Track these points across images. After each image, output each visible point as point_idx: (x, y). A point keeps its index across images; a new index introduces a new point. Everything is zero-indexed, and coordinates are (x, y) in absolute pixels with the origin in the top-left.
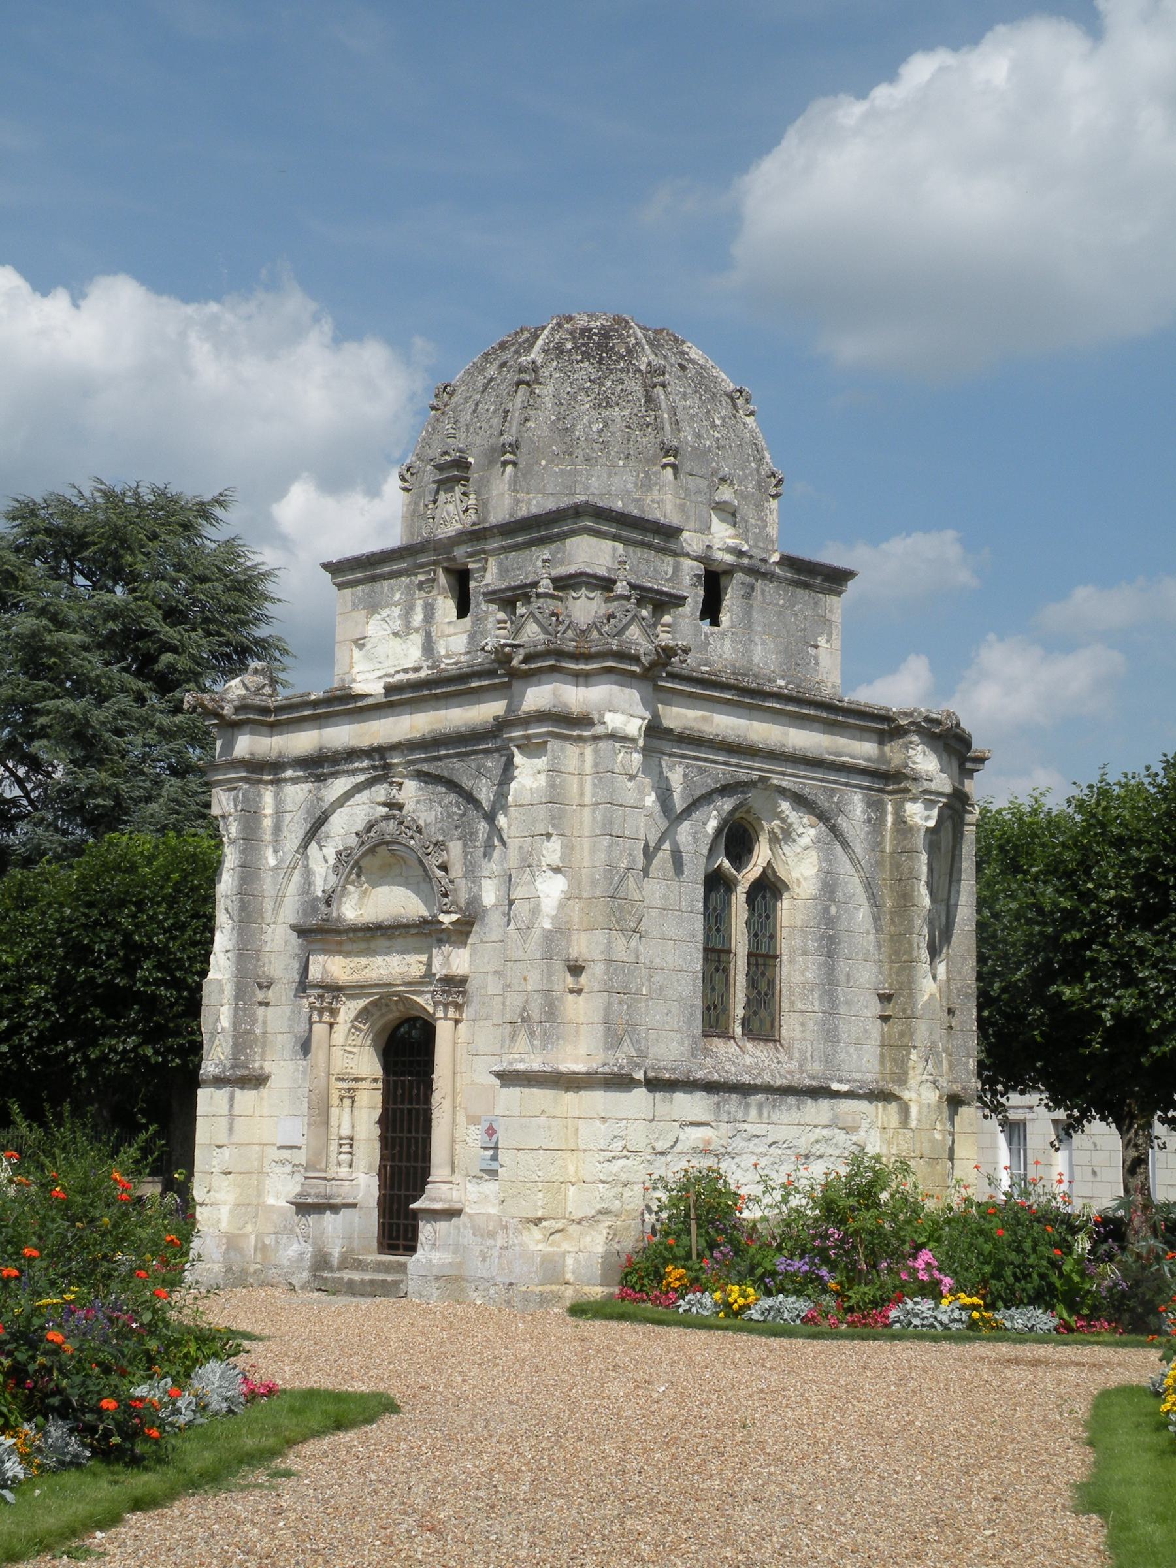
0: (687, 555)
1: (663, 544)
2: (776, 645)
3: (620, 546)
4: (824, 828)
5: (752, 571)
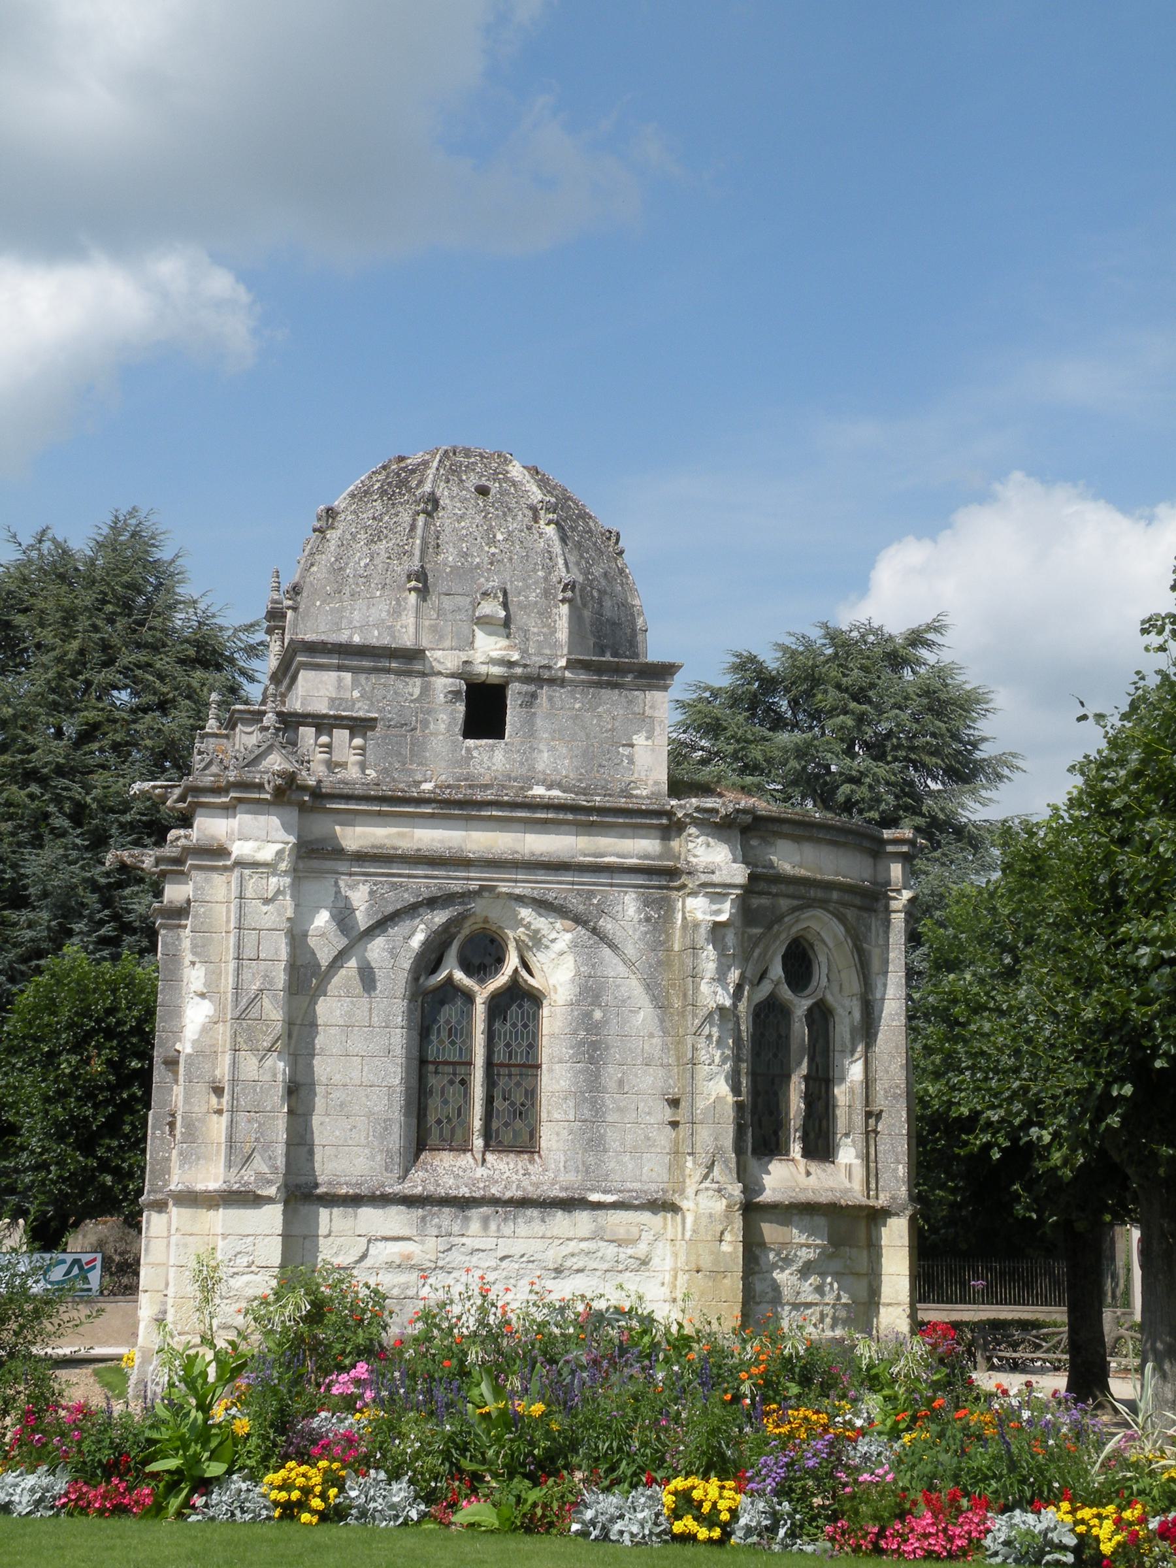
0: (440, 673)
1: (404, 667)
2: (571, 750)
3: (348, 676)
5: (527, 679)
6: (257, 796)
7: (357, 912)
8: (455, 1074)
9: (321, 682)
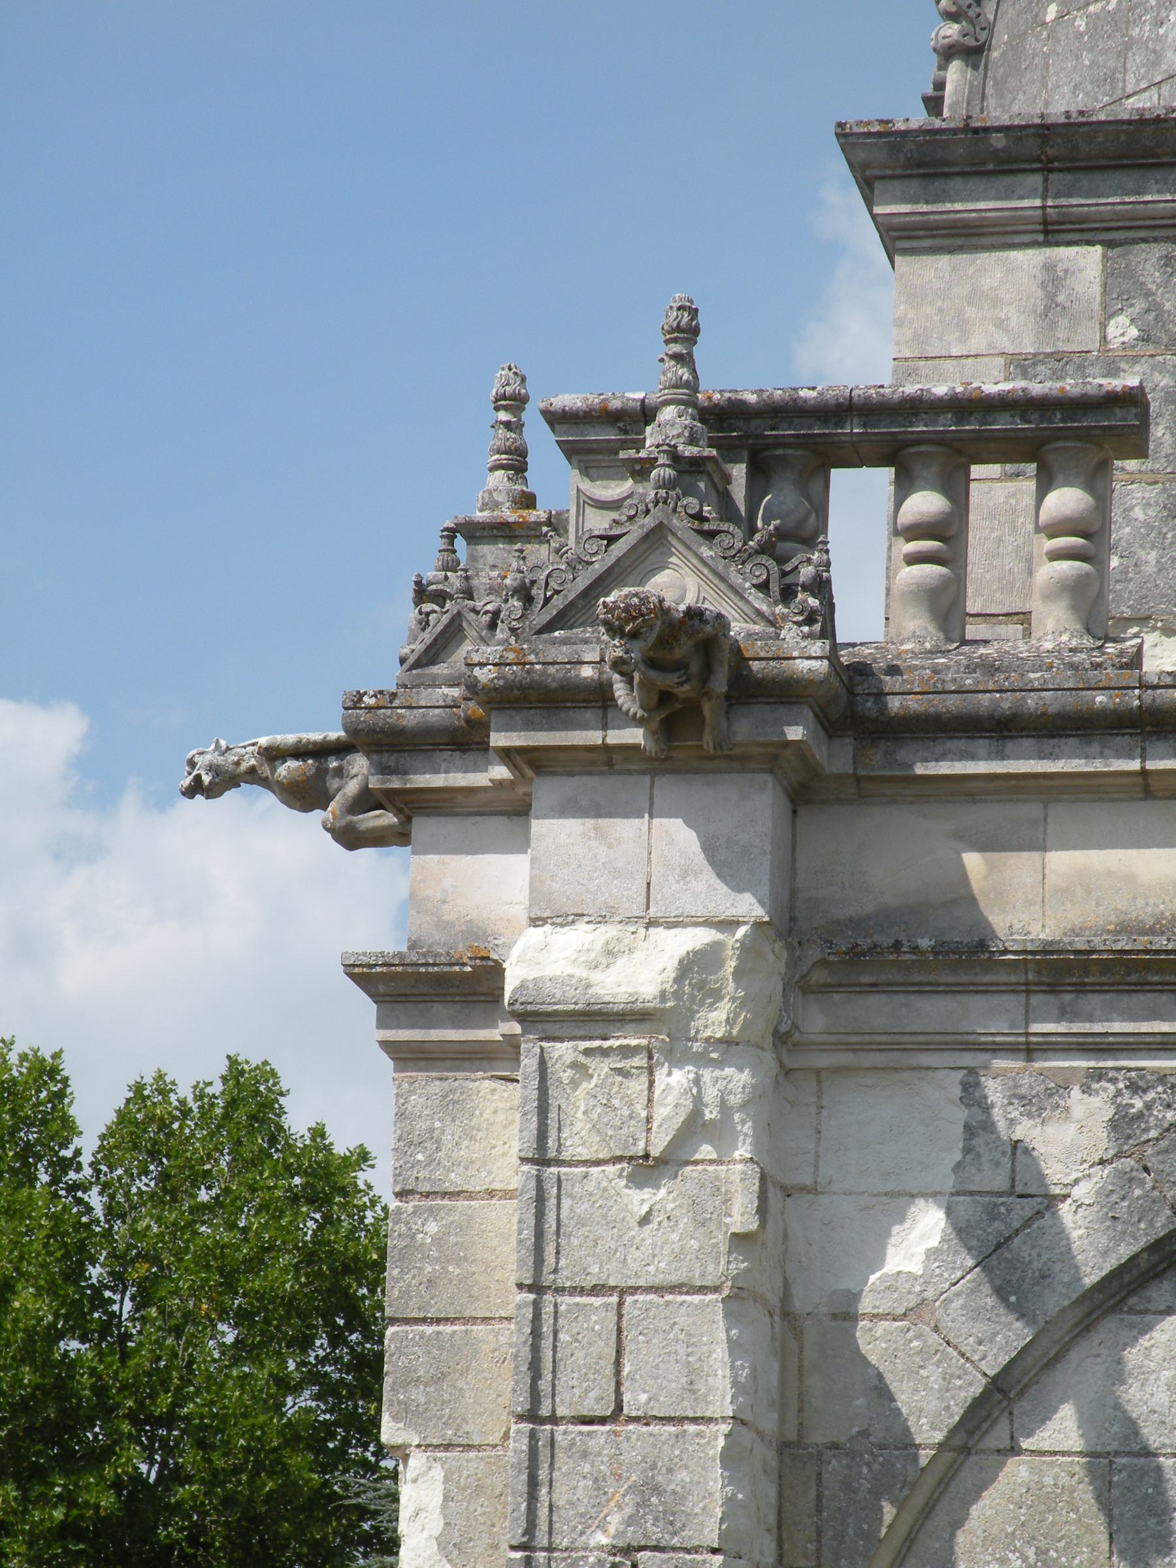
6: (593, 737)
7: (1065, 1208)
9: (976, 296)
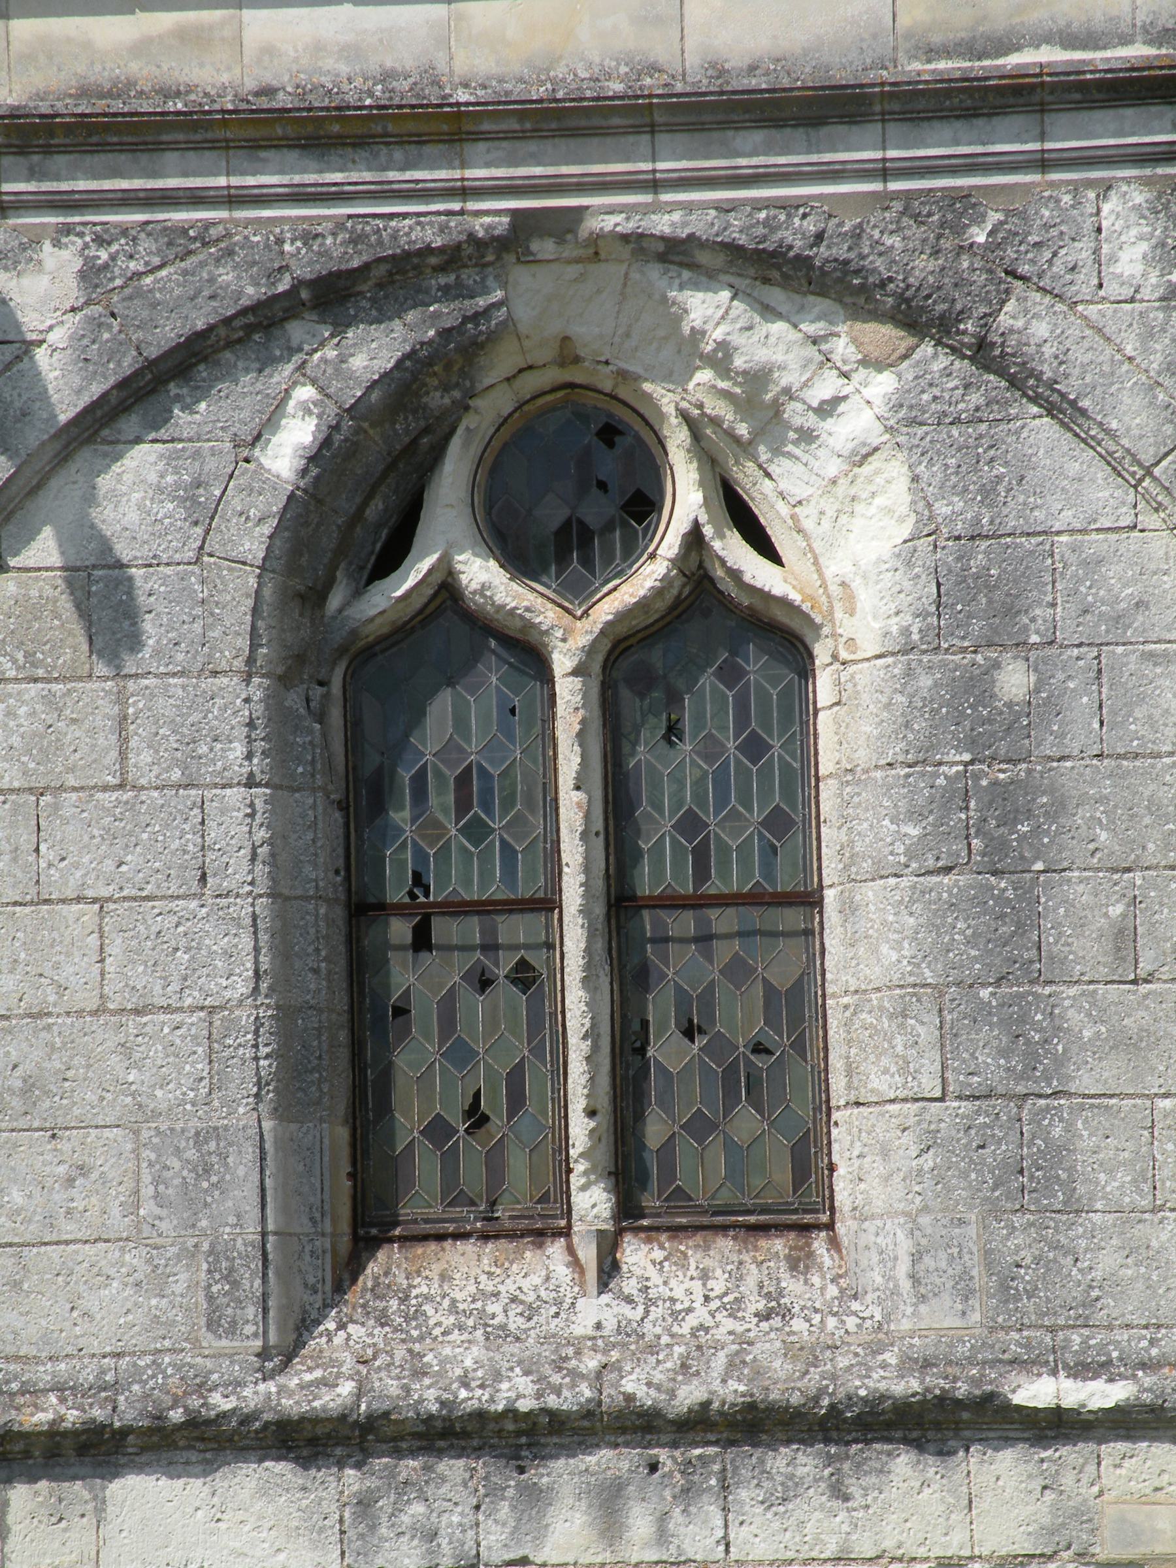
4: (943, 361)
7: (41, 354)
8: (490, 947)
